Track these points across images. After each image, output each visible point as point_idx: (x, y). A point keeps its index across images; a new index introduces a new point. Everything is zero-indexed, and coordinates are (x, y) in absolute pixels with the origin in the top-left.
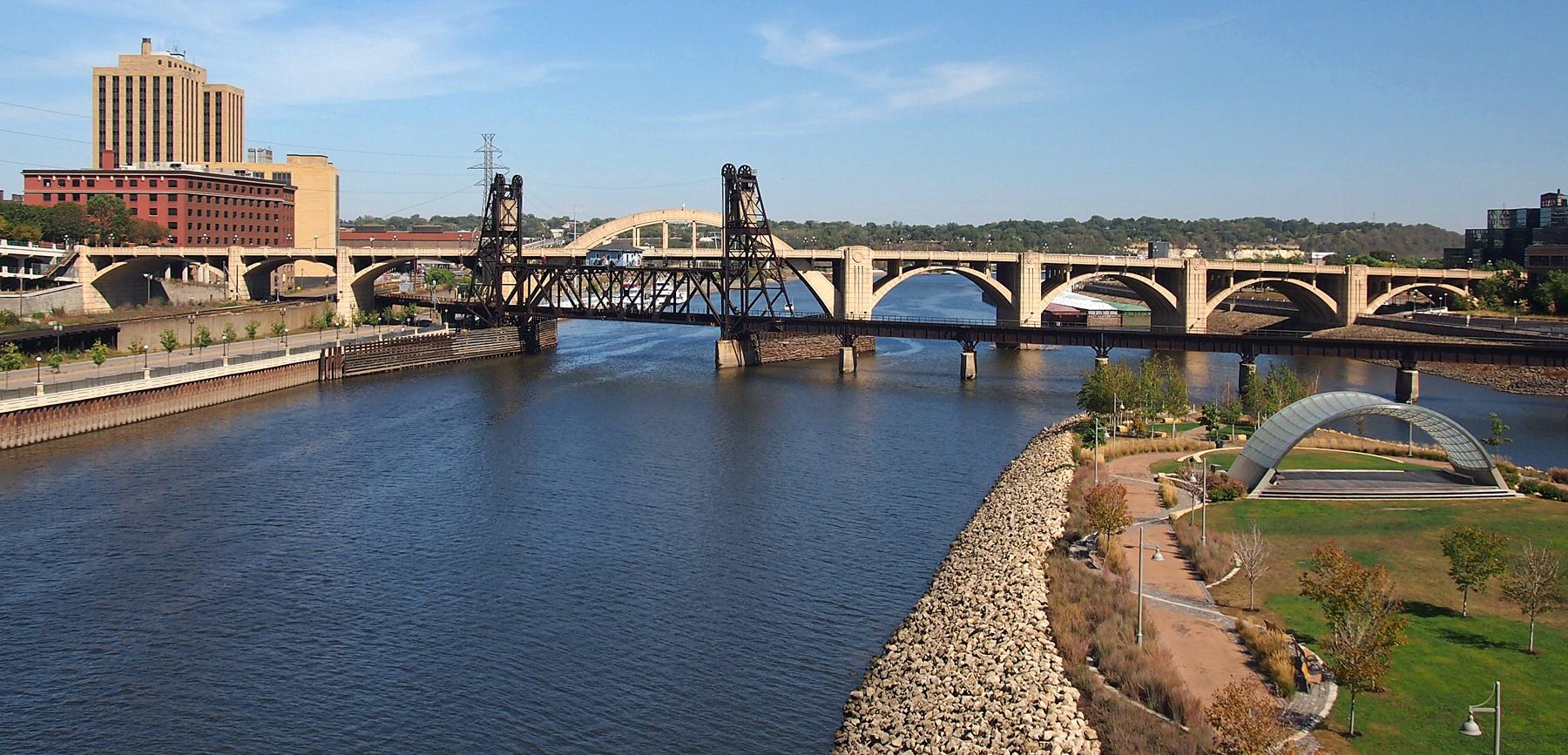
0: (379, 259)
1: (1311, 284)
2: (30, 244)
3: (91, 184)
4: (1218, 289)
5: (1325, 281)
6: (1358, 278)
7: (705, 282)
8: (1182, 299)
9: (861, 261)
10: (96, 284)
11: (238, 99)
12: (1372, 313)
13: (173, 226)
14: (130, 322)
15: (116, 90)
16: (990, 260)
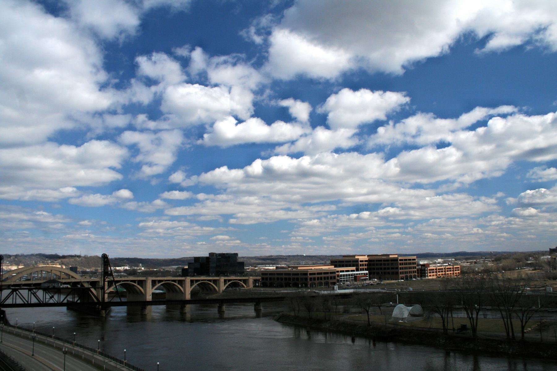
5: (215, 282)
8: (145, 290)
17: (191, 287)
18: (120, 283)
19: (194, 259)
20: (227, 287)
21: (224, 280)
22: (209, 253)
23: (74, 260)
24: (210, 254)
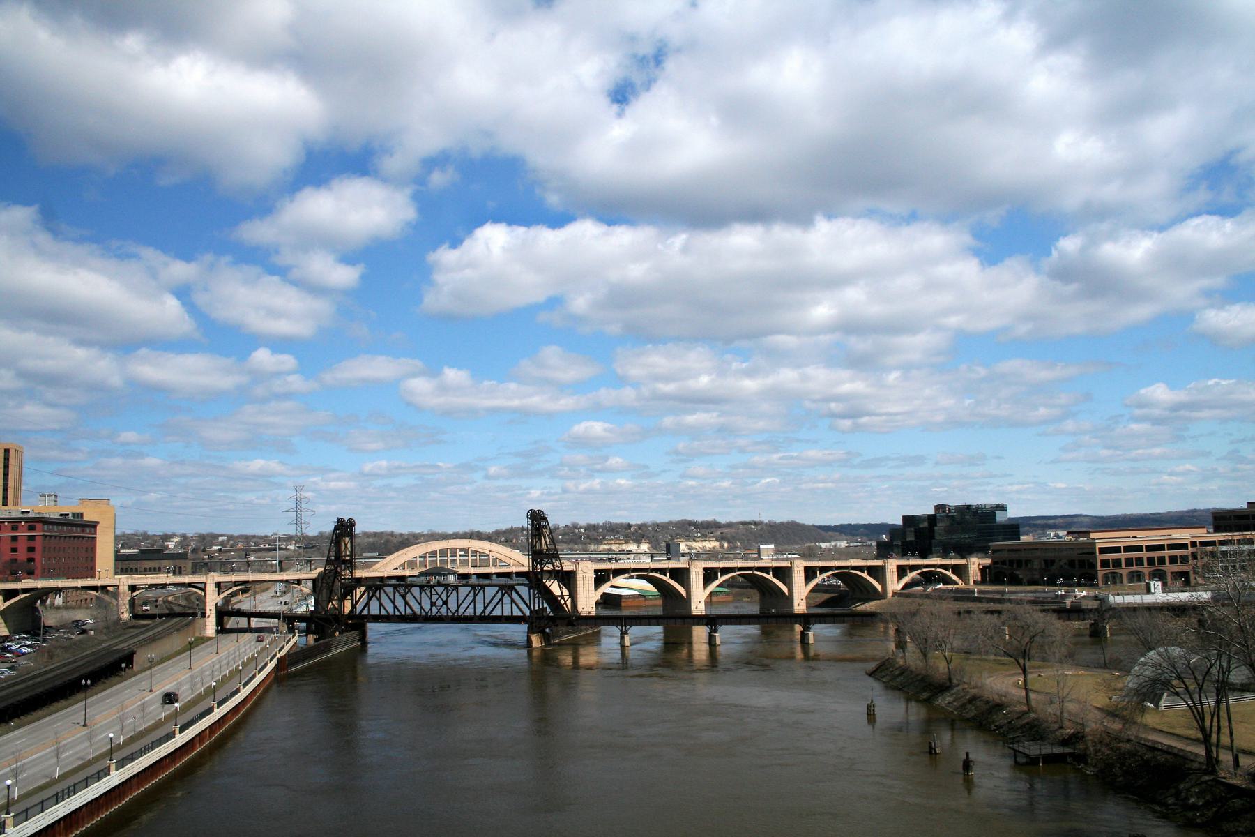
0: (236, 584)
1: (949, 571)
4: (710, 580)
5: (873, 571)
6: (798, 569)
8: (790, 590)
11: (20, 453)
12: (899, 589)
13: (31, 560)
16: (408, 575)
17: (705, 588)
18: (919, 571)
19: (928, 519)
20: (906, 587)
21: (899, 567)
22: (935, 506)
23: (747, 530)
24: (938, 508)
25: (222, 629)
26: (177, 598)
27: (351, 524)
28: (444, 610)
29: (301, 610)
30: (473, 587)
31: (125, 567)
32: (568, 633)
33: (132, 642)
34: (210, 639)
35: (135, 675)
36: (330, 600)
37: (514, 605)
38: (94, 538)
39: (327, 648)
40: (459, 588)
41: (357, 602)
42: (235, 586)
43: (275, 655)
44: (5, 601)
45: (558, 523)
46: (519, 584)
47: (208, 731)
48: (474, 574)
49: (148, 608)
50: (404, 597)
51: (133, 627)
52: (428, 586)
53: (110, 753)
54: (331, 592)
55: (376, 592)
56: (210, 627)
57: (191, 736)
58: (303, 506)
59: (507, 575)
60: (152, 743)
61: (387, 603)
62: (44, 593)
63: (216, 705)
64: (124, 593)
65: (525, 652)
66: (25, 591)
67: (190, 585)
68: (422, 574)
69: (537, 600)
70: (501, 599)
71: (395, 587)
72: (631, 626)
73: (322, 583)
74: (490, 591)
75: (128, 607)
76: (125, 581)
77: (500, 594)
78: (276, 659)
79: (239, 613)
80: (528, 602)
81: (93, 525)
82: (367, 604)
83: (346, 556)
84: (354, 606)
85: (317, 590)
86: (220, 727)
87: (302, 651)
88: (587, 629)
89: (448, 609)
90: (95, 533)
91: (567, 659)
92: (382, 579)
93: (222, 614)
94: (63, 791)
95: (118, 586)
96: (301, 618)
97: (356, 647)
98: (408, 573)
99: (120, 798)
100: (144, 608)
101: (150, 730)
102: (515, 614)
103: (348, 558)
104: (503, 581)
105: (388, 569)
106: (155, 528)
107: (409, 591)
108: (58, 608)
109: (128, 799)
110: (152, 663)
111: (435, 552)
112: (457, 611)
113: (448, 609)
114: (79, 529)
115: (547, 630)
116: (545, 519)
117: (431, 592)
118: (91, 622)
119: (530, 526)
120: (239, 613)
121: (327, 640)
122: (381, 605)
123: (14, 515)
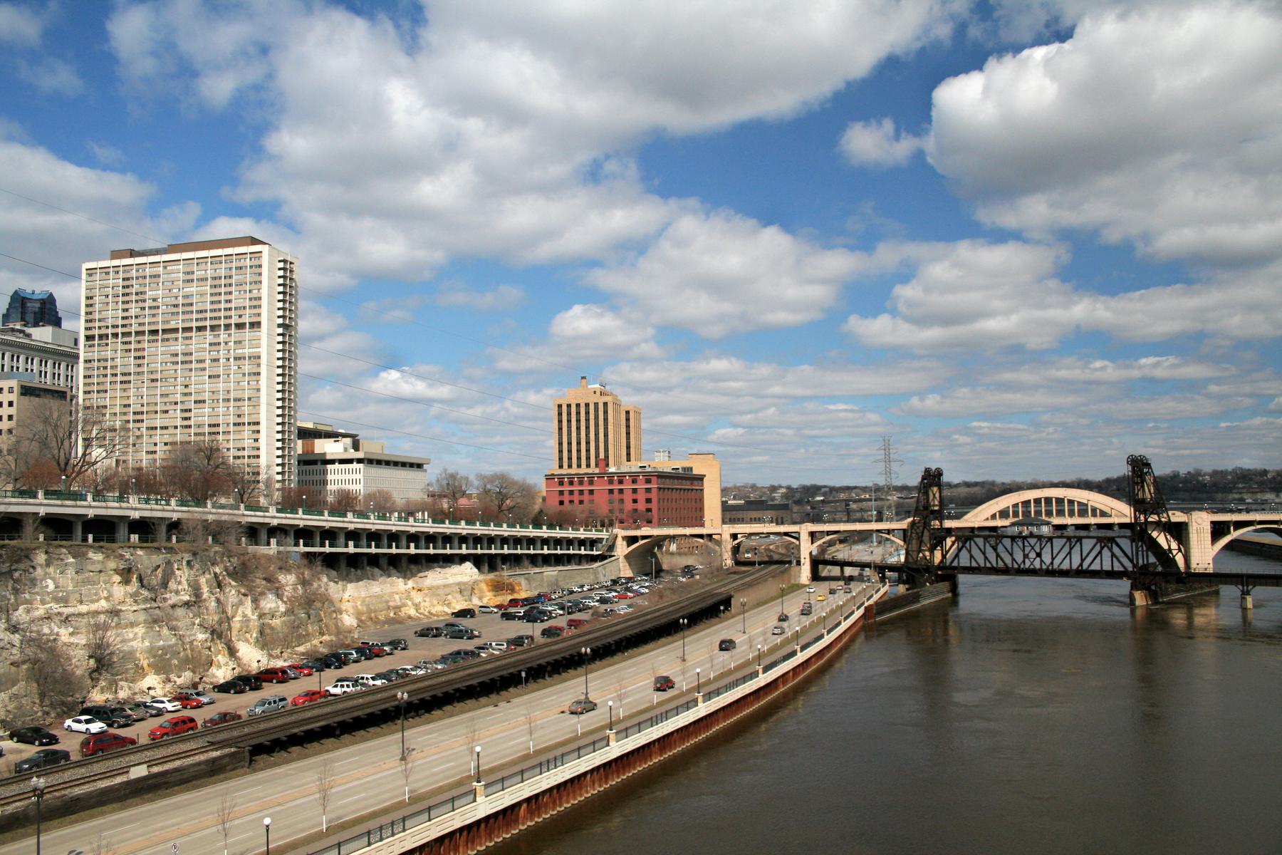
2: (545, 527)
3: (591, 483)
7: (968, 543)
9: (1200, 522)
10: (627, 557)
11: (638, 413)
13: (649, 510)
14: (737, 590)
15: (569, 414)
25: (816, 577)
26: (777, 547)
27: (939, 473)
28: (1037, 564)
29: (893, 560)
30: (1069, 539)
31: (753, 517)
32: (1178, 591)
33: (730, 586)
34: (805, 586)
35: (733, 617)
36: (920, 551)
37: (1114, 559)
38: (702, 490)
39: (916, 598)
40: (1054, 540)
41: (947, 552)
42: (828, 535)
43: (863, 603)
44: (629, 545)
45: (1177, 469)
46: (1118, 537)
47: (791, 674)
48: (1072, 525)
49: (750, 555)
50: (995, 549)
51: (735, 573)
52: (1020, 537)
53: (698, 688)
54: (921, 543)
55: (966, 543)
56: (805, 572)
57: (774, 677)
58: (891, 456)
59: (1109, 527)
60: (737, 680)
61: (977, 554)
62: (659, 541)
63: (799, 649)
64: (726, 541)
65: (1127, 610)
66: (644, 537)
67: (786, 534)
68: (1013, 524)
69: (1140, 553)
70: (1100, 553)
71: (986, 538)
72: (1254, 586)
73: (912, 533)
74: (1088, 544)
75: (730, 553)
76: (728, 530)
77: (1098, 548)
78: (863, 608)
79: (834, 563)
80: (1130, 554)
81: (700, 478)
82: (957, 556)
83: (934, 505)
84: (944, 556)
85: (907, 539)
86: (804, 670)
87: (891, 600)
88: (1202, 588)
89: (1042, 561)
90: (703, 485)
91: (1178, 618)
92: (972, 529)
93: (816, 563)
94: (657, 716)
95: (721, 535)
96: (892, 568)
97: (946, 598)
98: (999, 523)
99: (708, 727)
100: (746, 555)
101: (738, 668)
102: (1115, 569)
103: (936, 508)
104: (1102, 533)
105: (978, 519)
106: (764, 481)
107: (1000, 542)
108: (672, 554)
109: (714, 730)
110: (744, 609)
111: (1029, 501)
112: (1052, 563)
113: (1042, 561)
114: (688, 482)
115: (1153, 587)
116: (1148, 465)
117: (1023, 543)
118: (258, 580)
119: (1130, 474)
120: (834, 563)
121: (915, 590)
122: (971, 557)
123: (634, 470)
